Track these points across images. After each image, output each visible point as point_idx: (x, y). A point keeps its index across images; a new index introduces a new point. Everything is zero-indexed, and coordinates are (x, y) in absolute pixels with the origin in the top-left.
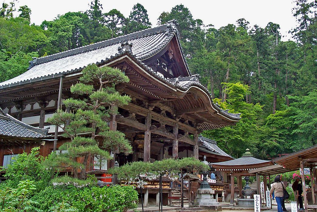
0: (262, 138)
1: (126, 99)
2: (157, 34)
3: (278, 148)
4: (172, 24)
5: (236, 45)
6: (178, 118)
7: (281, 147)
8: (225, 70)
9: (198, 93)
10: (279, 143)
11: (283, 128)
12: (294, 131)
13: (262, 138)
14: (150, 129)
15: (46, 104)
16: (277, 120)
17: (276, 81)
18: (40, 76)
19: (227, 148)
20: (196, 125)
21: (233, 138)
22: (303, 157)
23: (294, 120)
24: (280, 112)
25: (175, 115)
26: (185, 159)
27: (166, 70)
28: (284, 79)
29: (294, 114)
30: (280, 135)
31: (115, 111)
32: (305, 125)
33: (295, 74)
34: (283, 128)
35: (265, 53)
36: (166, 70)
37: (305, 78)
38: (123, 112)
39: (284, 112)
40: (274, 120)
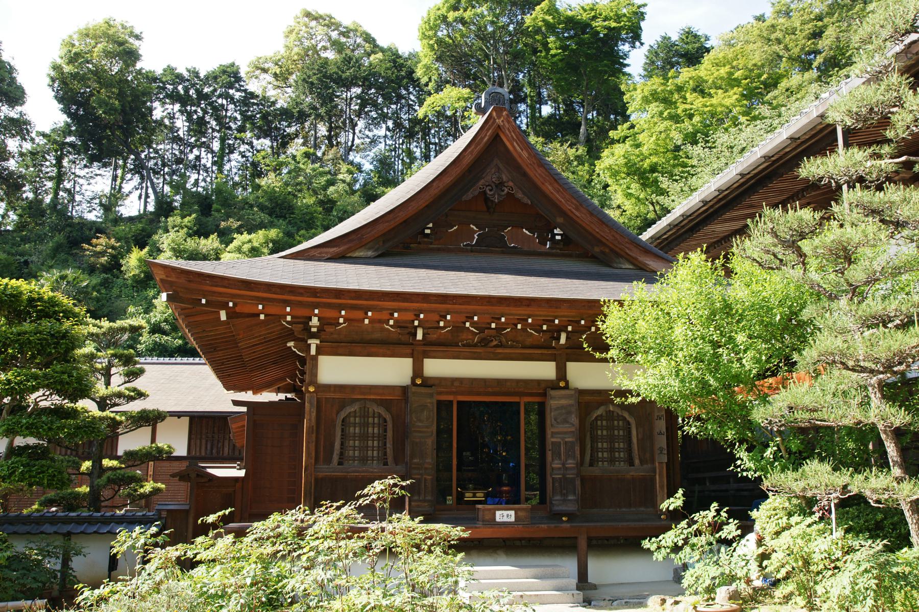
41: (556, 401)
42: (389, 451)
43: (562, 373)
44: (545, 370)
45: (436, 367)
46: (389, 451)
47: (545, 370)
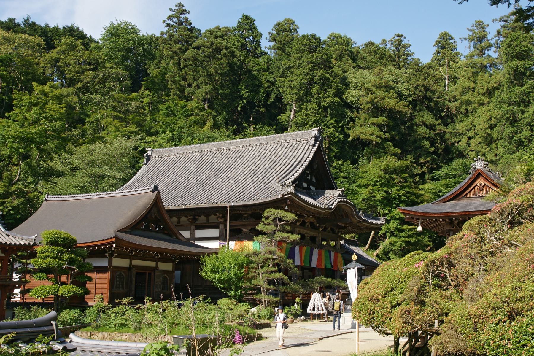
6: (322, 228)
9: (343, 207)
20: (338, 232)
25: (318, 225)
27: (309, 178)
36: (309, 178)
41: (157, 273)
42: (125, 286)
43: (157, 264)
44: (153, 264)
45: (135, 262)
46: (125, 286)
47: (153, 264)
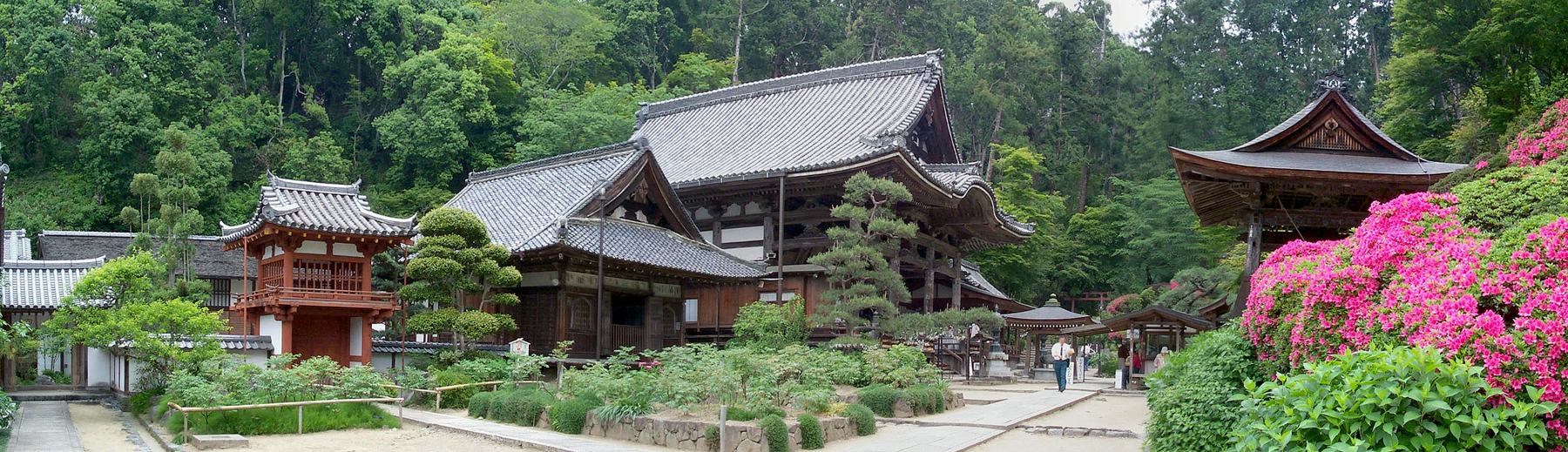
0: (1056, 261)
1: (911, 229)
2: (906, 75)
3: (1084, 280)
4: (934, 58)
5: (1021, 56)
7: (1092, 280)
8: (995, 111)
10: (1087, 271)
11: (1097, 243)
12: (1118, 251)
13: (1056, 261)
14: (900, 254)
15: (722, 211)
16: (1089, 226)
17: (1092, 139)
18: (737, 172)
19: (997, 278)
21: (1009, 260)
22: (1135, 319)
23: (1118, 229)
24: (1096, 211)
26: (973, 310)
28: (1107, 135)
29: (1121, 218)
30: (1091, 256)
31: (895, 245)
32: (1137, 242)
33: (1130, 130)
34: (1097, 243)
35: (1076, 79)
37: (1150, 145)
38: (905, 243)
39: (1101, 211)
40: (1082, 226)
